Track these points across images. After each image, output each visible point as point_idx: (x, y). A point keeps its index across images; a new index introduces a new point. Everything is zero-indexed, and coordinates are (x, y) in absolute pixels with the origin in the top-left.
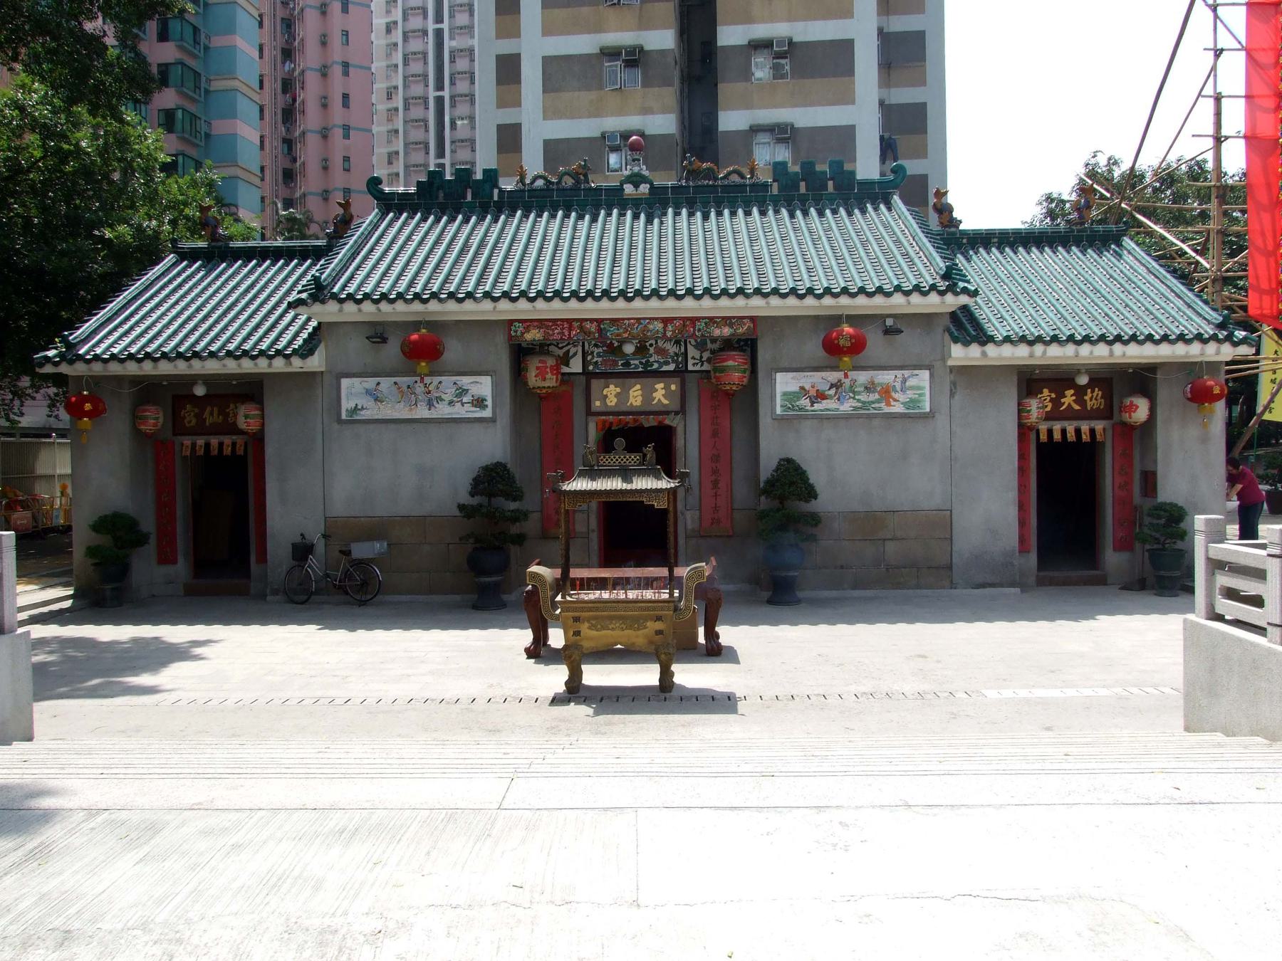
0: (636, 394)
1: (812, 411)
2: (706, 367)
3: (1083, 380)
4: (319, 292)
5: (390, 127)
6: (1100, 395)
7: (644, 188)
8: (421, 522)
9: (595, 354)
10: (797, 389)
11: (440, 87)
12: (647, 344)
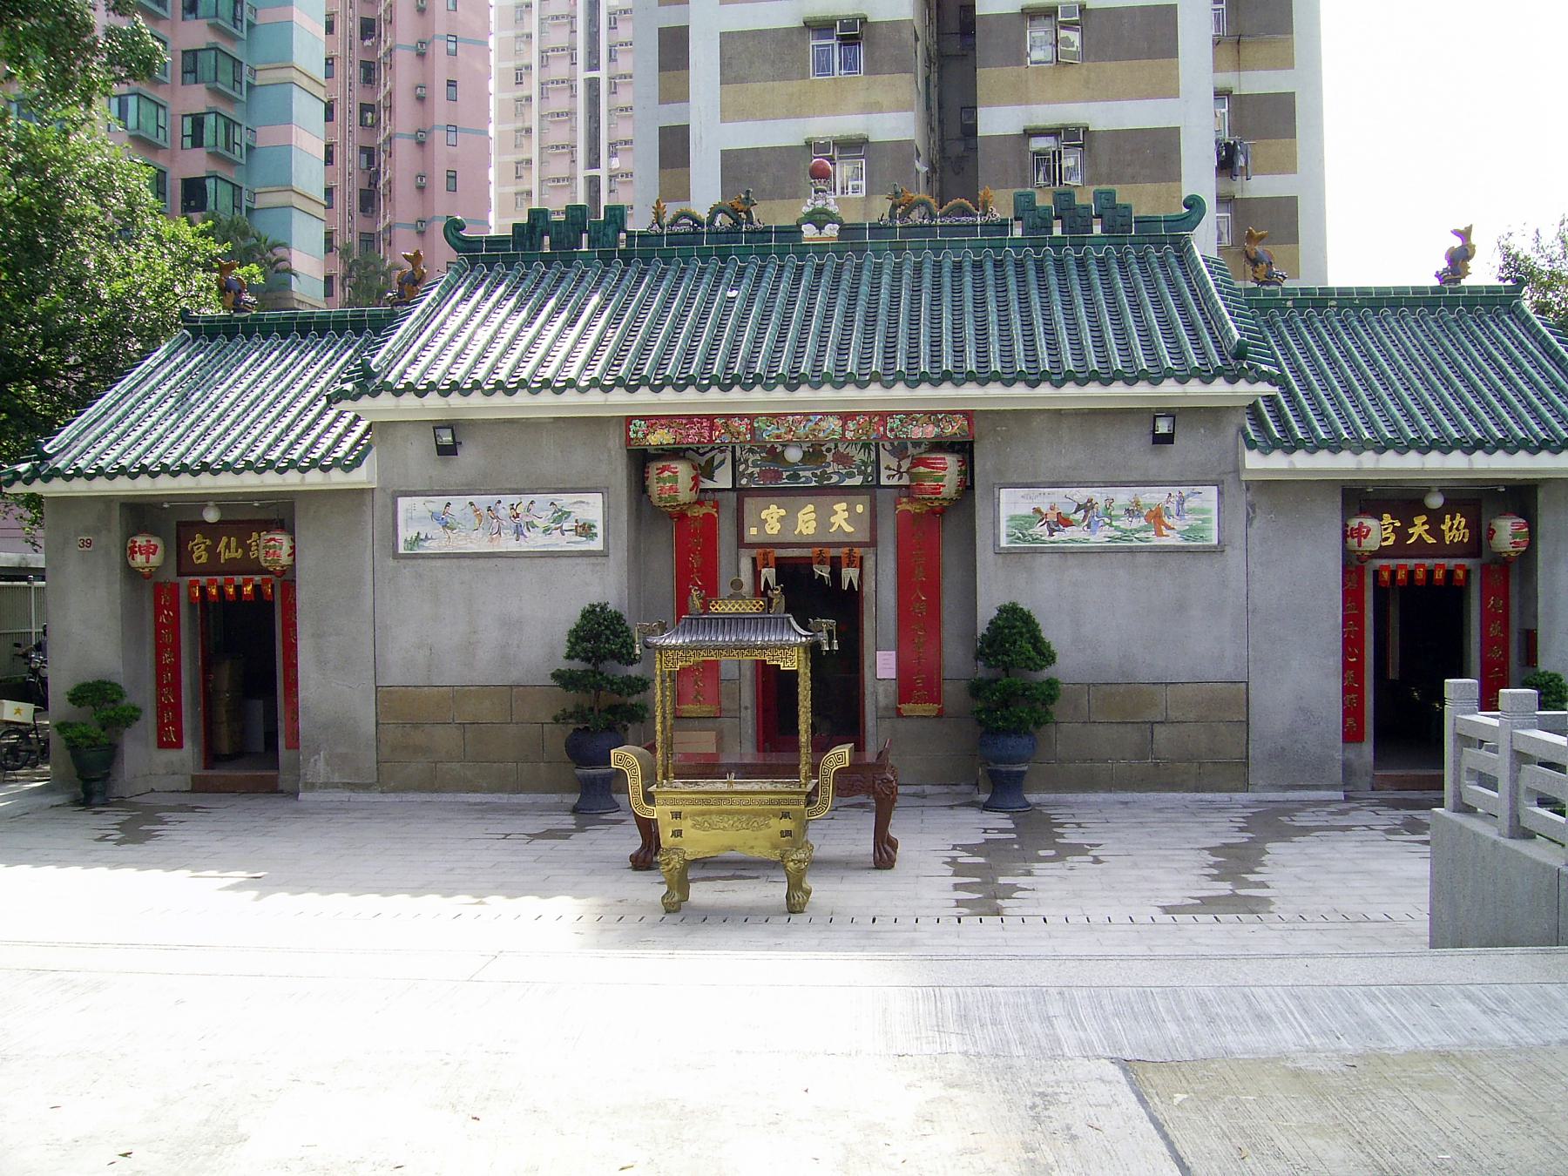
0: (806, 518)
1: (1051, 542)
2: (905, 481)
3: (1435, 501)
4: (367, 382)
5: (519, 125)
6: (1463, 524)
7: (831, 230)
8: (512, 691)
9: (750, 462)
10: (1030, 512)
11: (593, 66)
12: (824, 449)
